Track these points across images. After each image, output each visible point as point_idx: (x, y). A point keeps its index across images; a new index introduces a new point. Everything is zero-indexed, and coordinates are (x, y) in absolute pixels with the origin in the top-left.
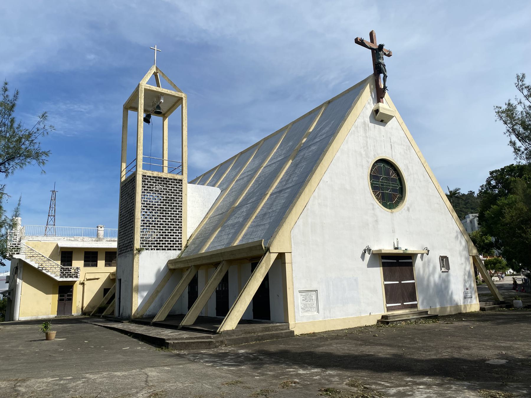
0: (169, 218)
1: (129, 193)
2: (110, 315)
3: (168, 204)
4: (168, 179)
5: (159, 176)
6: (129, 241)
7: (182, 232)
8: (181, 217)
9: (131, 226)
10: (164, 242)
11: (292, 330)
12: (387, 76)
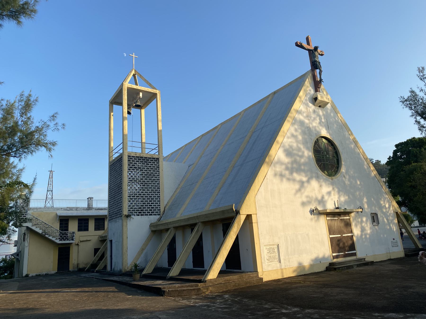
0: (150, 189)
1: (117, 170)
2: (102, 269)
3: (149, 178)
4: (148, 158)
5: (141, 156)
6: (118, 209)
7: (161, 200)
8: (159, 188)
9: (120, 197)
10: (146, 209)
11: (261, 277)
12: (322, 71)
